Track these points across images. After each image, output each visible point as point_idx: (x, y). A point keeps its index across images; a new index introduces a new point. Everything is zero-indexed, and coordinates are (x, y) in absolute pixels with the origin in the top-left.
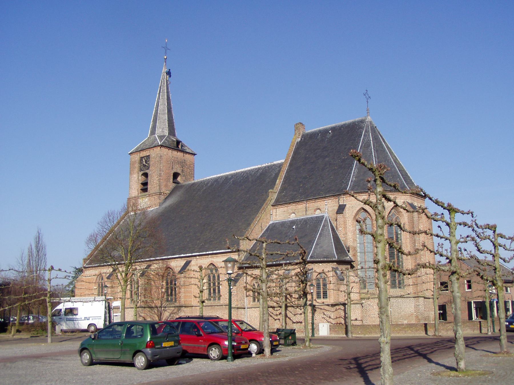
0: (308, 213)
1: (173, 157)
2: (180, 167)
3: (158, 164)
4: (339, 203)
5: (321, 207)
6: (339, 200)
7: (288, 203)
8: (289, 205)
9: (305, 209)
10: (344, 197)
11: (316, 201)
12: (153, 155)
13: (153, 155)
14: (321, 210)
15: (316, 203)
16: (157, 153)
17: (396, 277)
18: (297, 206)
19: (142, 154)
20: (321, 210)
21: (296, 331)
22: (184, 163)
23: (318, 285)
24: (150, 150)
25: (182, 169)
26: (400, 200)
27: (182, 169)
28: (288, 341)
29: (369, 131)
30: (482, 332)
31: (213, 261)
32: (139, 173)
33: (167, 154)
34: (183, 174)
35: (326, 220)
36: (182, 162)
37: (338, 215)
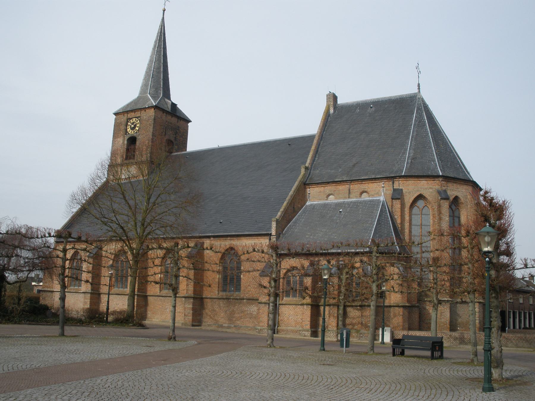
0: (351, 196)
1: (167, 121)
2: (173, 134)
3: (150, 127)
4: (393, 187)
5: (369, 190)
6: (393, 183)
7: (316, 183)
8: (327, 185)
9: (348, 191)
10: (399, 181)
11: (364, 182)
12: (145, 117)
13: (145, 117)
14: (368, 193)
15: (362, 184)
16: (151, 114)
17: (287, 283)
18: (338, 186)
19: (130, 115)
20: (368, 193)
21: (443, 340)
22: (178, 130)
23: (289, 283)
24: (141, 111)
25: (175, 136)
26: (462, 189)
27: (175, 136)
28: (435, 352)
29: (422, 108)
30: (65, 334)
31: (234, 245)
32: (124, 137)
33: (161, 117)
34: (176, 142)
35: (383, 205)
36: (176, 129)
37: (394, 200)
